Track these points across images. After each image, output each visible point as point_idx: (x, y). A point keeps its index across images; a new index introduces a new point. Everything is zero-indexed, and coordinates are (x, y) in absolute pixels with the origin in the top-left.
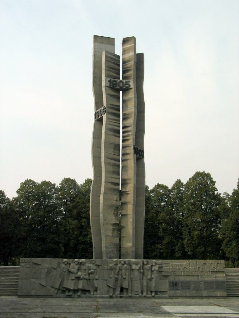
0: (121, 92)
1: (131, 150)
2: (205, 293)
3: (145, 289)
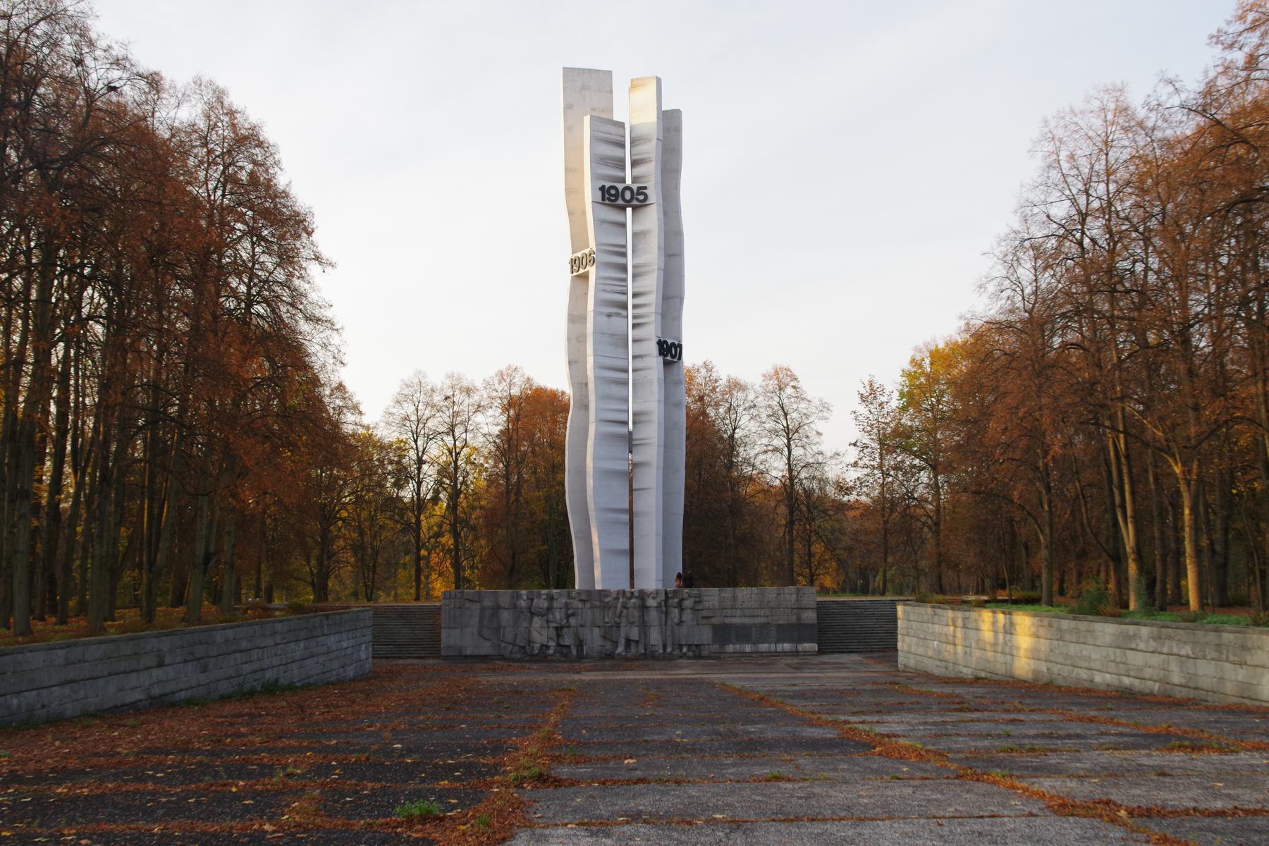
0: (629, 210)
2: (972, 598)
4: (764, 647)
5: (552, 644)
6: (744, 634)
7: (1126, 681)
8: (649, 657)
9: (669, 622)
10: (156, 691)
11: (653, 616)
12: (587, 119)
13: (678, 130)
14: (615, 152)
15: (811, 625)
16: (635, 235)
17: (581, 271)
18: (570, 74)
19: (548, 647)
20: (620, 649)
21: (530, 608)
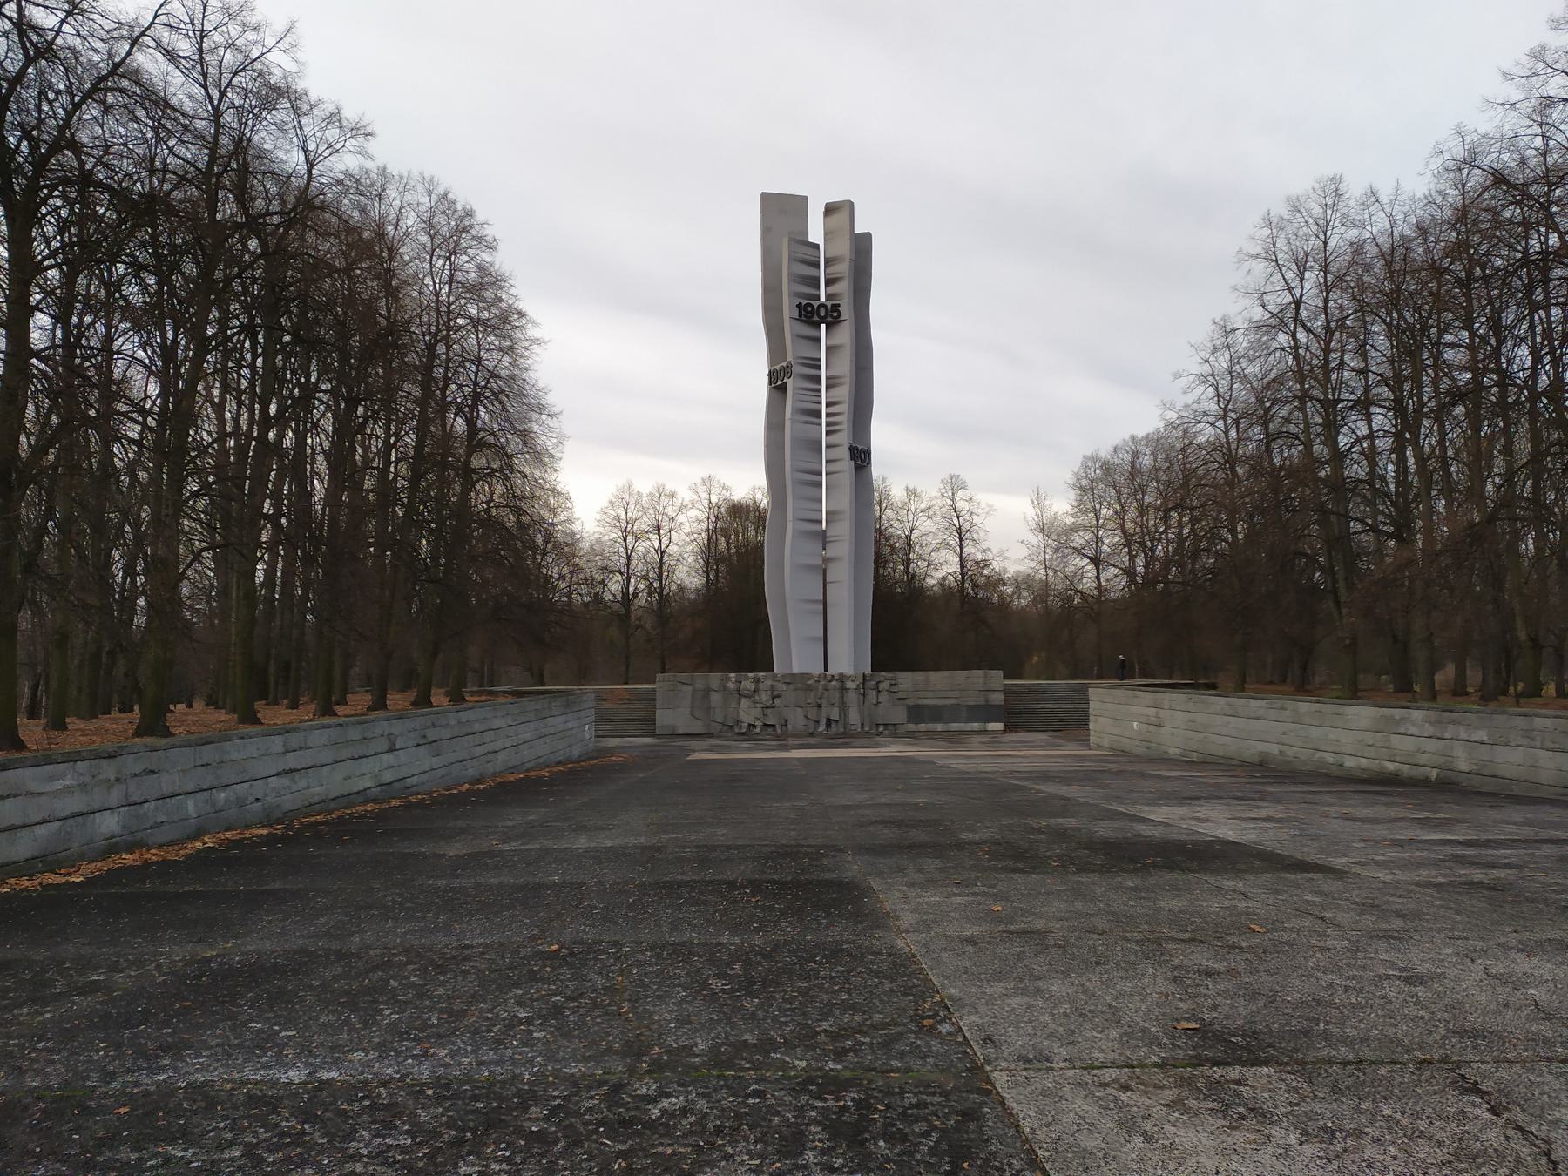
0: (823, 326)
1: (844, 453)
4: (955, 726)
5: (758, 723)
6: (936, 714)
7: (1391, 766)
10: (388, 777)
11: (852, 697)
14: (808, 271)
16: (828, 348)
18: (768, 200)
20: (822, 728)
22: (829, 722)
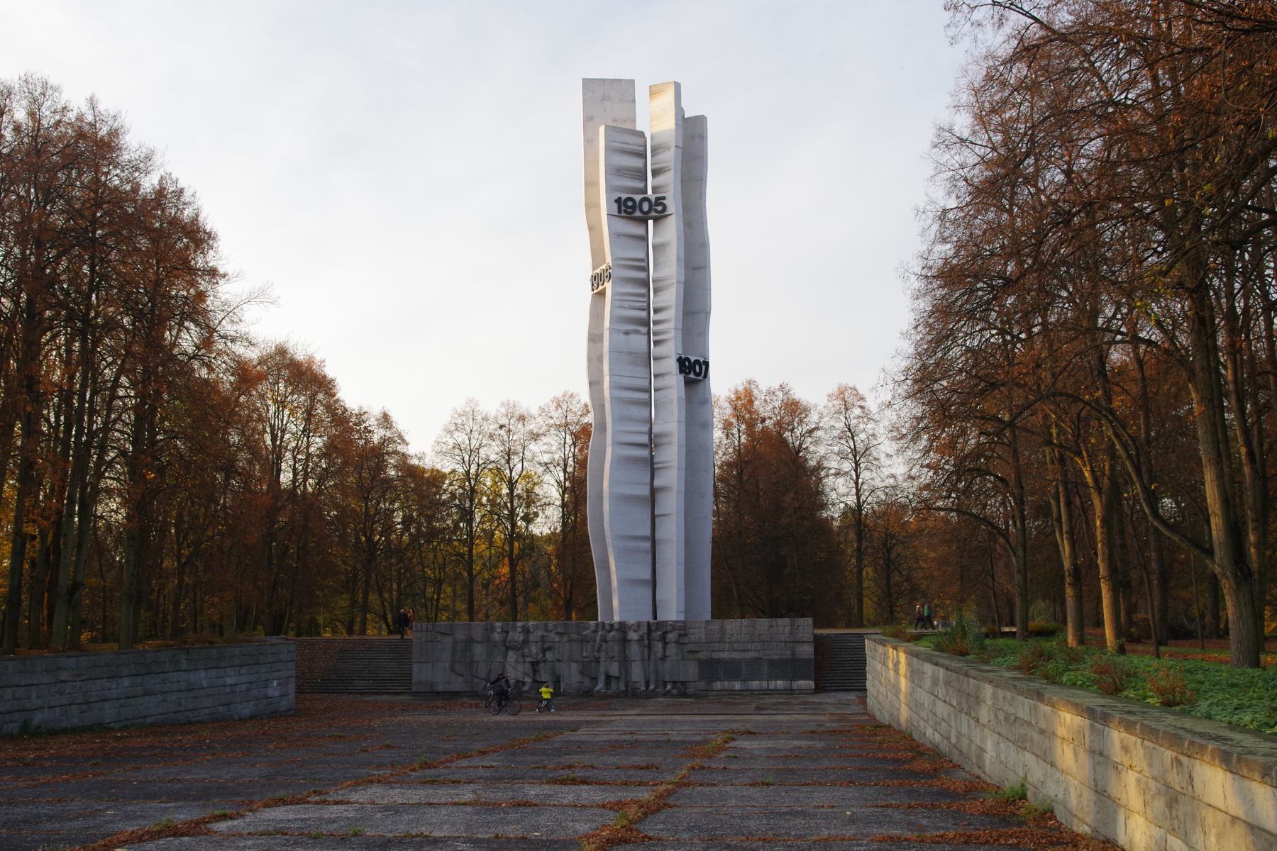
3: (652, 678)
4: (755, 684)
5: (528, 680)
6: (732, 670)
8: (631, 695)
9: (653, 657)
11: (634, 649)
12: (602, 129)
13: (702, 137)
15: (808, 661)
17: (601, 288)
19: (524, 683)
20: (600, 686)
21: (504, 642)
22: (609, 678)
